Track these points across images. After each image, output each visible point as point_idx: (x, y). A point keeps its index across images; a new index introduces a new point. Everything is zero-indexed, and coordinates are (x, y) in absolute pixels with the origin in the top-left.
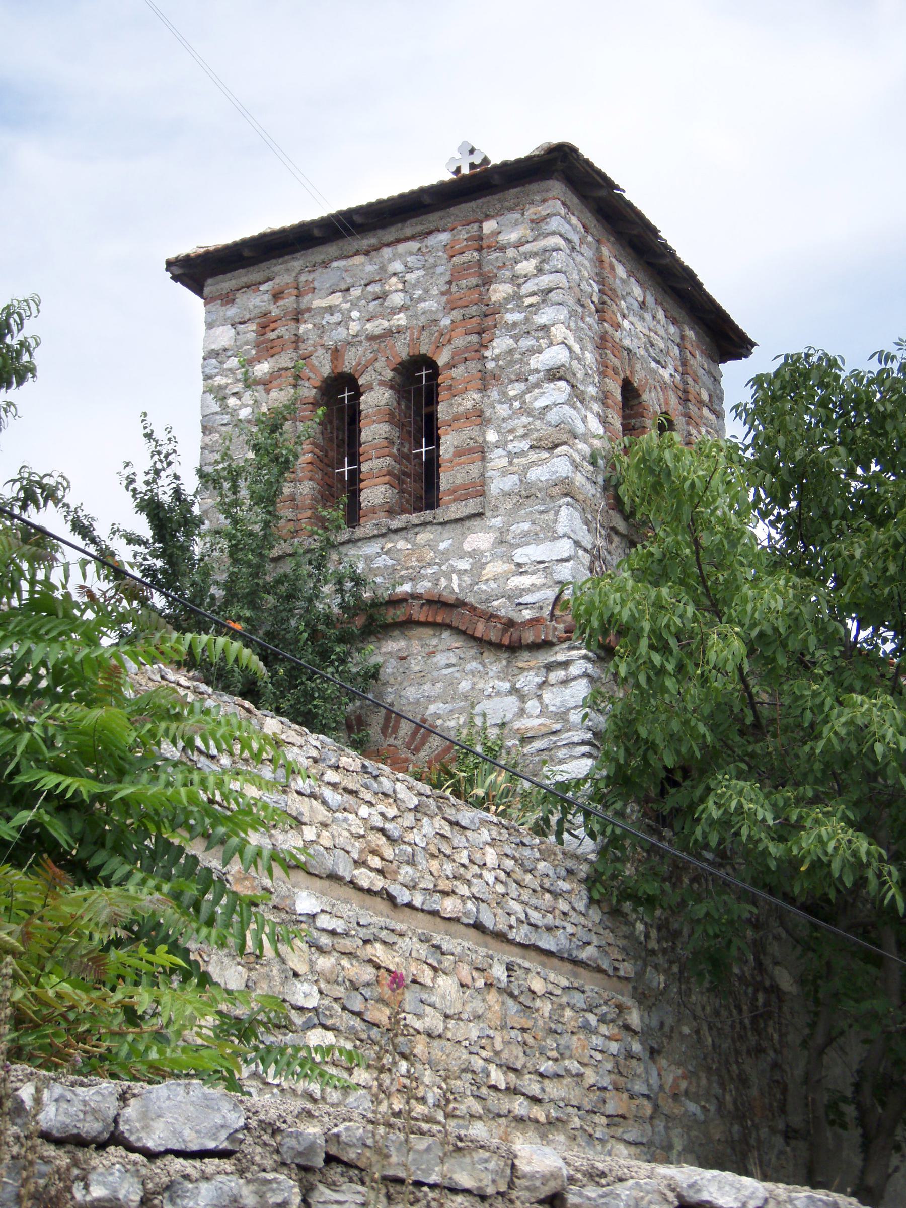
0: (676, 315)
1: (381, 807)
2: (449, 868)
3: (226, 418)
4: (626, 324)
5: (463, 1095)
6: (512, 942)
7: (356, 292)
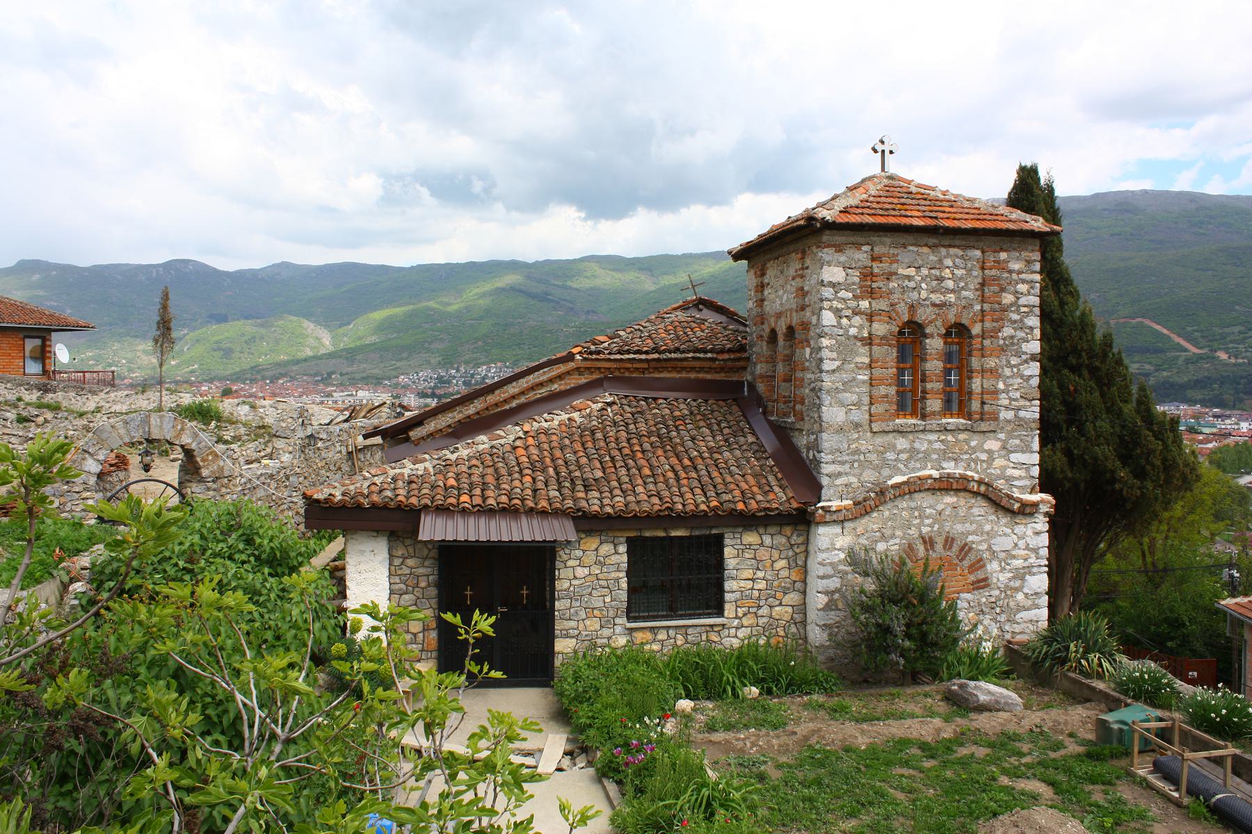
0: (902, 241)
7: (925, 271)
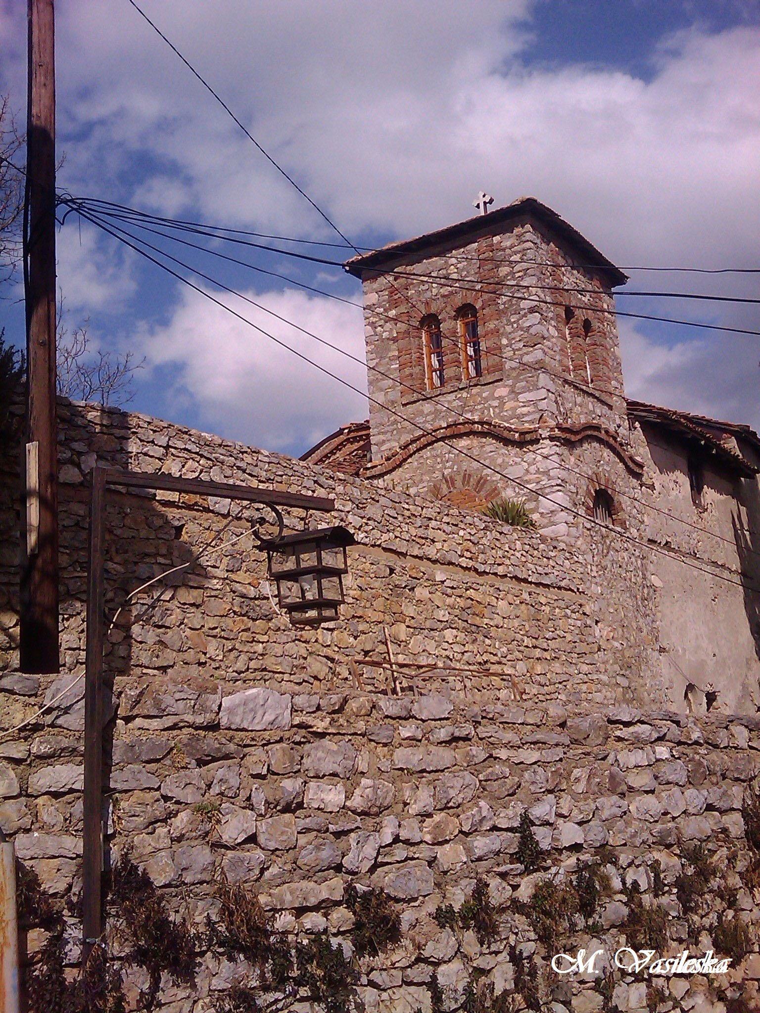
1: (468, 530)
2: (500, 553)
3: (377, 338)
4: (565, 279)
5: (513, 651)
6: (531, 583)
